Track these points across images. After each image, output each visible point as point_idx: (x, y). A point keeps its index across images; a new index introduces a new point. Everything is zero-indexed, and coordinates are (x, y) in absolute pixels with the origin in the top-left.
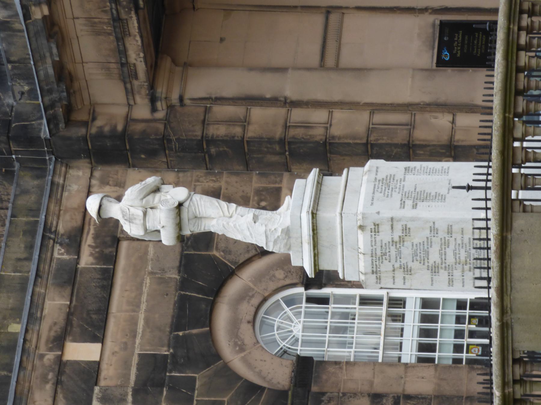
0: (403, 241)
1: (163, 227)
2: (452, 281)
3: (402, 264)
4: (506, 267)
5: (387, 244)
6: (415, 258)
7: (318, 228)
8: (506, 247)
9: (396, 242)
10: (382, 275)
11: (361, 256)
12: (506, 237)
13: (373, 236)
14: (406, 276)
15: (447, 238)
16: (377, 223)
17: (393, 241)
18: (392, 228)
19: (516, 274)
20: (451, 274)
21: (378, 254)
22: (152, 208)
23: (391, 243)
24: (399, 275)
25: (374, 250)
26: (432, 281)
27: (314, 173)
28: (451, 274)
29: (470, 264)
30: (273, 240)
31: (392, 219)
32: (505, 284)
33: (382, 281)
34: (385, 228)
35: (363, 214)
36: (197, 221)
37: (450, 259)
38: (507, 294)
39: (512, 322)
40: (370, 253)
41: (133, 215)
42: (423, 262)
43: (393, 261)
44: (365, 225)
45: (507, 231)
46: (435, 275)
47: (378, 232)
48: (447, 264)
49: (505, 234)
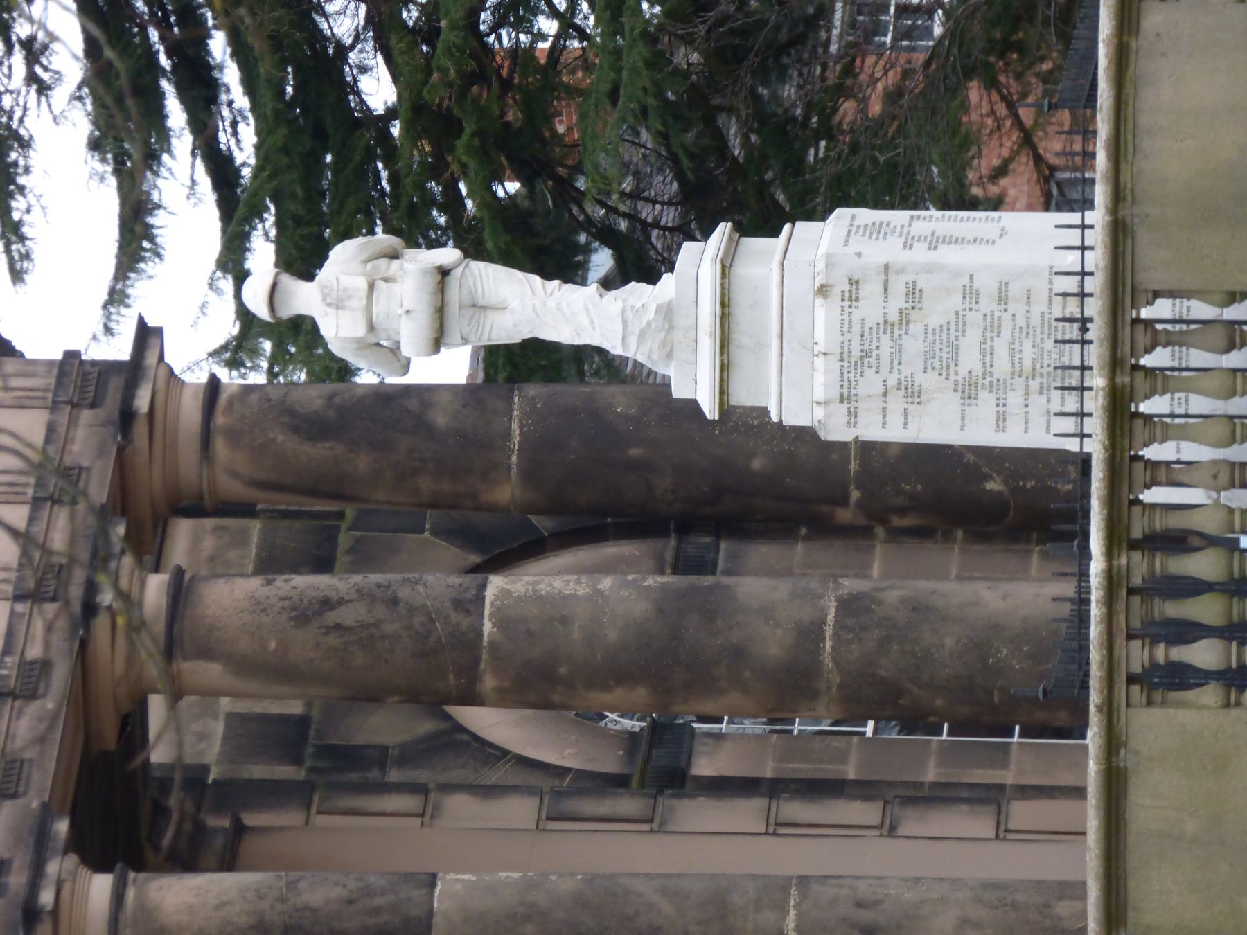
0: (908, 322)
1: (408, 312)
2: (1004, 420)
3: (902, 377)
4: (1126, 104)
5: (874, 330)
6: (929, 362)
7: (732, 303)
8: (1127, 66)
9: (893, 325)
10: (860, 405)
11: (820, 362)
12: (1128, 43)
13: (847, 310)
14: (911, 407)
15: (997, 314)
16: (855, 278)
17: (886, 322)
18: (886, 290)
19: (1144, 120)
20: (1002, 401)
21: (853, 353)
22: (386, 280)
23: (882, 326)
24: (896, 403)
25: (846, 343)
26: (963, 418)
27: (723, 230)
28: (1002, 401)
29: (1042, 376)
30: (637, 331)
31: (886, 267)
32: (1122, 138)
33: (861, 419)
34: (871, 290)
35: (829, 256)
36: (477, 314)
37: (1002, 366)
38: (1126, 157)
39: (1133, 225)
40: (838, 350)
41: (346, 289)
42: (945, 371)
43: (884, 370)
44: (830, 282)
45: (1129, 34)
46: (970, 405)
47: (857, 300)
48: (996, 376)
49: (1125, 38)
